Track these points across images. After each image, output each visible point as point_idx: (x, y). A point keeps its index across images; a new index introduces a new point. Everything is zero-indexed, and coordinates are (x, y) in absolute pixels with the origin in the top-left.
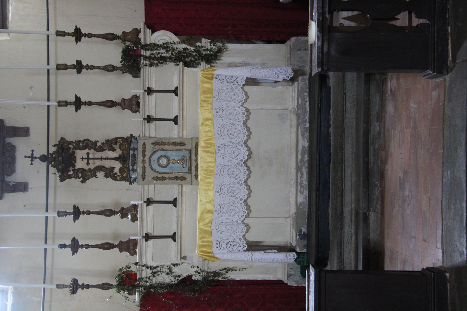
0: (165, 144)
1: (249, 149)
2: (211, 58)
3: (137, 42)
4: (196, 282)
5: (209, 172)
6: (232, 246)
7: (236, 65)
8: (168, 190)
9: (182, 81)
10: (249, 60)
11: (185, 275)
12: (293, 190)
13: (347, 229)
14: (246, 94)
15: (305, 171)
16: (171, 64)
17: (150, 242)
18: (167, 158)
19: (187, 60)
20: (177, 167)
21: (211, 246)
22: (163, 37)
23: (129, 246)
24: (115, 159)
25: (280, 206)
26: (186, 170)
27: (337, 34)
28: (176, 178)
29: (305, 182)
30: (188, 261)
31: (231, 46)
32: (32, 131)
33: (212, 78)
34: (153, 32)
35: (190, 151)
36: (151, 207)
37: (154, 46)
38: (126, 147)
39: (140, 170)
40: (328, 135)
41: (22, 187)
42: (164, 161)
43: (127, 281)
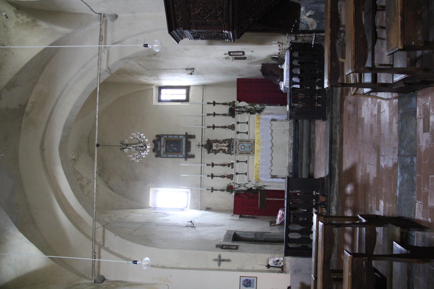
0: (243, 141)
1: (272, 143)
2: (259, 111)
3: (234, 105)
4: (254, 190)
5: (258, 151)
6: (266, 176)
7: (269, 114)
8: (244, 158)
9: (249, 119)
10: (273, 112)
11: (250, 187)
12: (288, 158)
13: (303, 170)
14: (271, 124)
15: (292, 151)
16: (246, 114)
17: (238, 176)
18: (243, 146)
19: (251, 112)
20: (248, 150)
21: (259, 176)
22: (243, 104)
23: (231, 177)
24: (226, 146)
25: (283, 163)
26: (251, 150)
27: (295, 109)
28: (247, 153)
29: (292, 155)
30: (251, 182)
31: (267, 107)
32: (196, 137)
33: (260, 119)
34: (240, 102)
35: (252, 144)
36: (238, 163)
37: (240, 107)
38: (230, 142)
39: (234, 150)
40: (298, 139)
41: (193, 156)
42: (243, 147)
43: (230, 189)
